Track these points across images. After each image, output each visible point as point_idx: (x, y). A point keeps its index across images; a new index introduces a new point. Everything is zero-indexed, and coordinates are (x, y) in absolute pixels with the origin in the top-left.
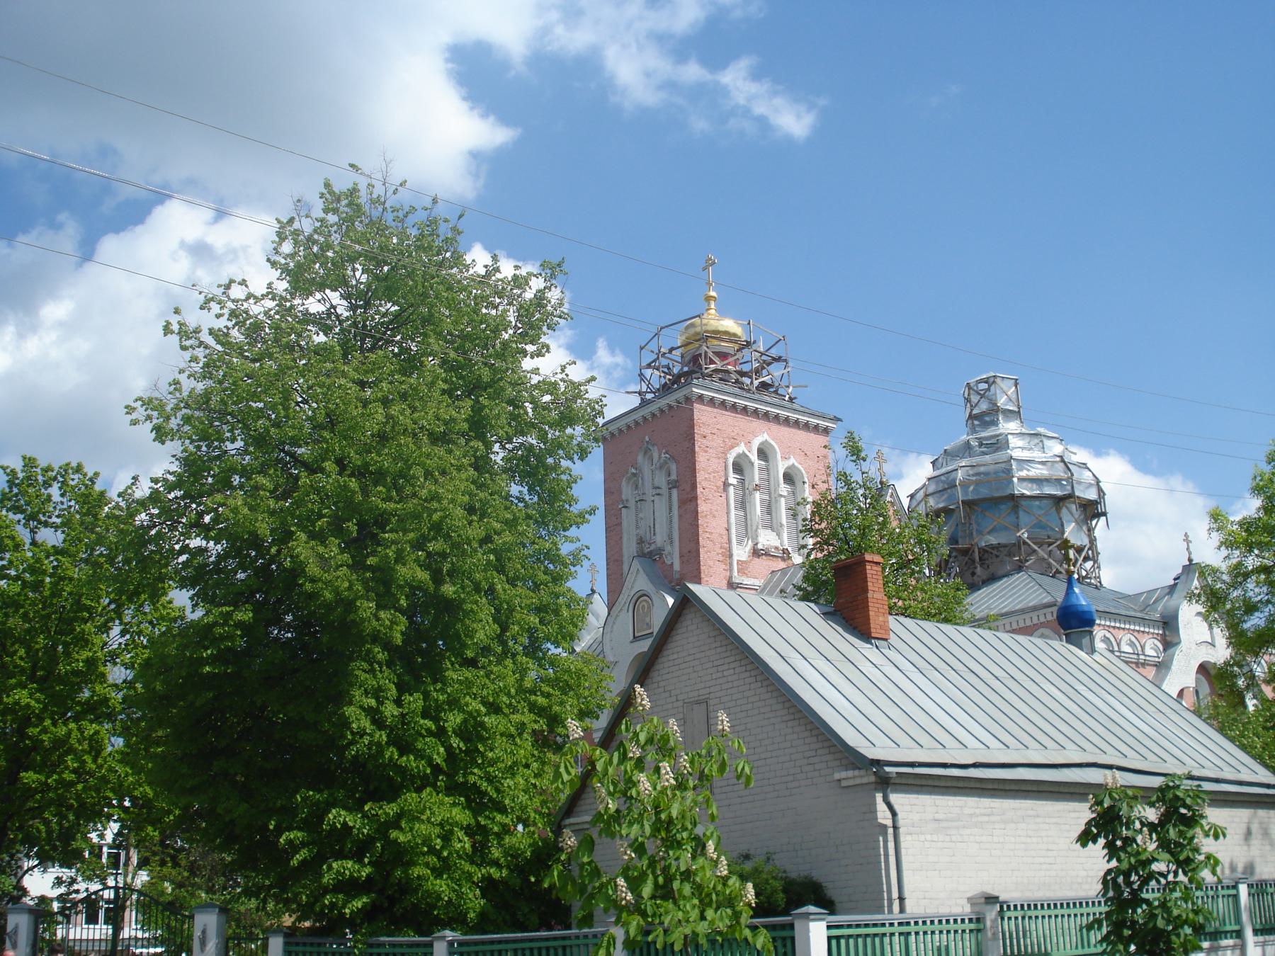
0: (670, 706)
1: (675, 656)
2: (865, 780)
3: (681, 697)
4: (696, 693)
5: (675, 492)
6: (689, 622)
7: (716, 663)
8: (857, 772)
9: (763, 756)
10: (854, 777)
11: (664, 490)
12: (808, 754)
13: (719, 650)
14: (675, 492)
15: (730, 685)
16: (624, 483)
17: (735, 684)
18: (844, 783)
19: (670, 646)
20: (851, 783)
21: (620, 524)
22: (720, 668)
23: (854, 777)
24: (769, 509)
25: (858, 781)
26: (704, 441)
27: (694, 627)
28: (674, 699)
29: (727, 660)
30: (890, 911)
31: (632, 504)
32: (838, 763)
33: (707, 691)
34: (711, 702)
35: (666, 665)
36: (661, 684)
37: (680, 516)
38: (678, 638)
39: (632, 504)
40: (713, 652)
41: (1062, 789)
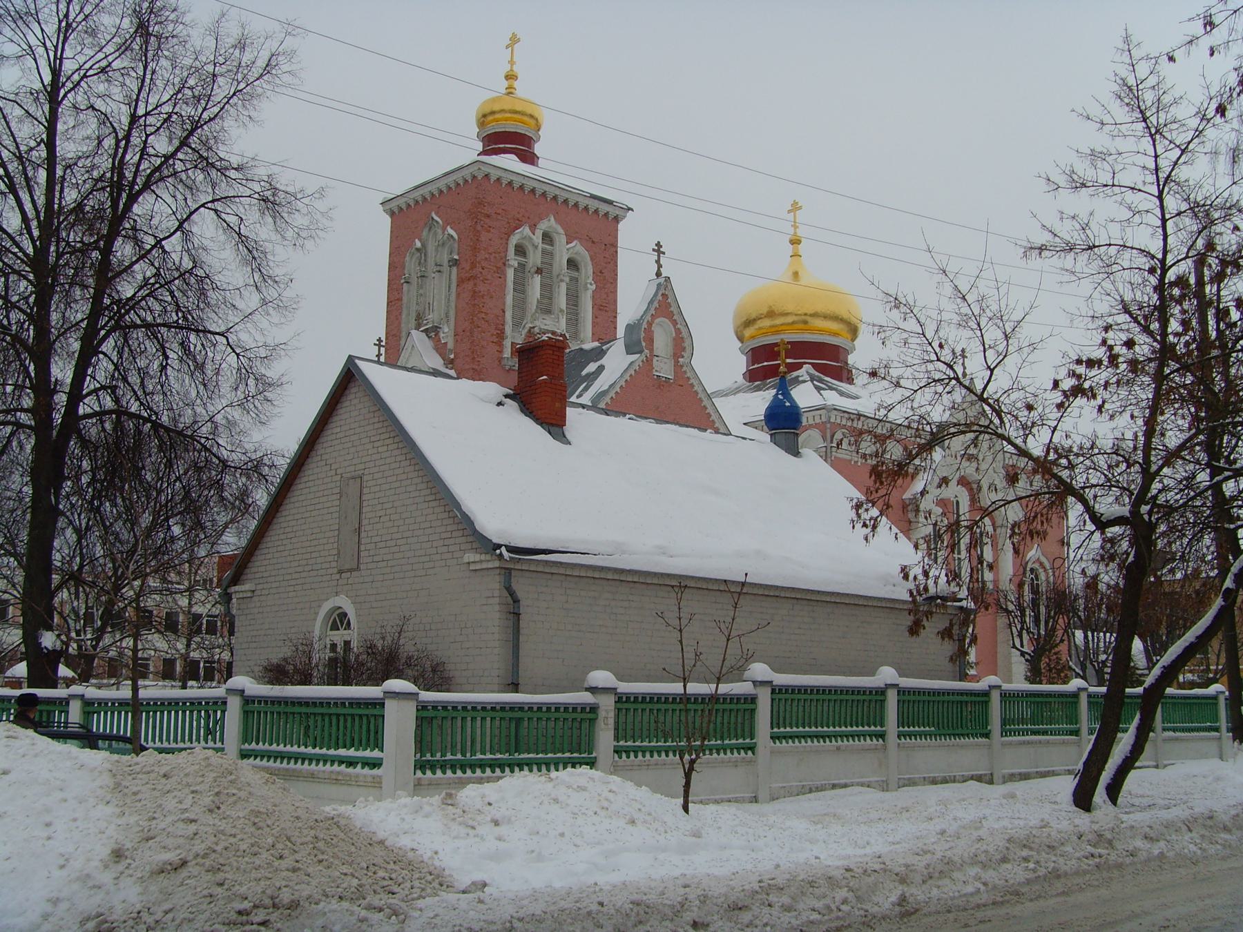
0: (329, 480)
1: (338, 430)
2: (490, 565)
3: (339, 472)
4: (352, 468)
5: (455, 269)
6: (352, 396)
7: (373, 439)
8: (483, 557)
9: (405, 535)
10: (481, 561)
11: (446, 268)
12: (444, 536)
13: (376, 426)
14: (455, 269)
15: (382, 462)
16: (407, 258)
17: (388, 461)
18: (472, 567)
19: (335, 418)
20: (478, 567)
21: (400, 299)
22: (376, 444)
23: (481, 561)
24: (548, 291)
25: (485, 566)
26: (487, 221)
27: (356, 401)
28: (333, 472)
29: (383, 437)
30: (1164, 729)
31: (414, 280)
32: (469, 546)
33: (362, 466)
34: (365, 478)
35: (329, 438)
36: (324, 457)
37: (458, 295)
38: (341, 411)
39: (414, 280)
40: (371, 427)
41: (897, 606)
